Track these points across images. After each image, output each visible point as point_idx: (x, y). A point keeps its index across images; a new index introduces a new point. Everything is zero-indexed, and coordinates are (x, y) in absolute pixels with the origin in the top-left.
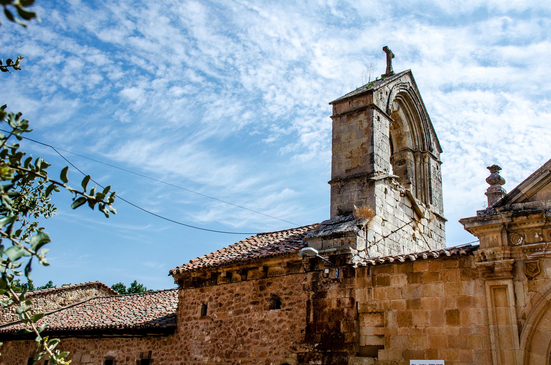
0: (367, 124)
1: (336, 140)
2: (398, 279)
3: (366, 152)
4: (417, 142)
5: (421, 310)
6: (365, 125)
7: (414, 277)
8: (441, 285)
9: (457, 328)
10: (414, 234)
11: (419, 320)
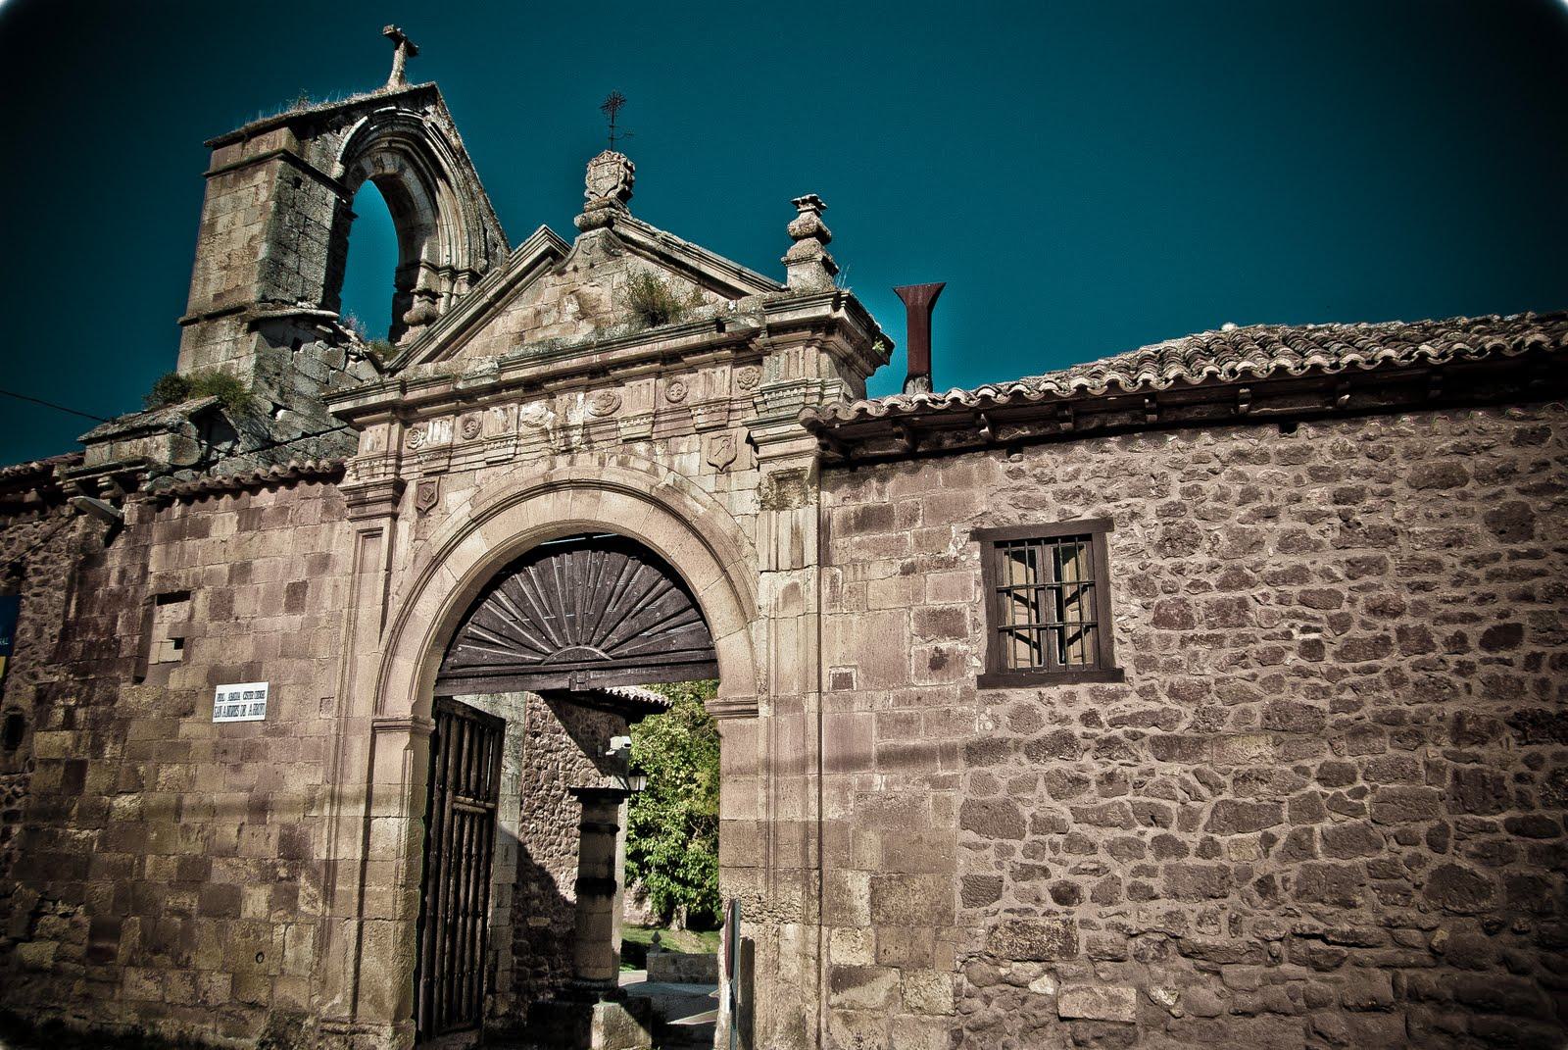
3: (255, 254)
9: (298, 618)
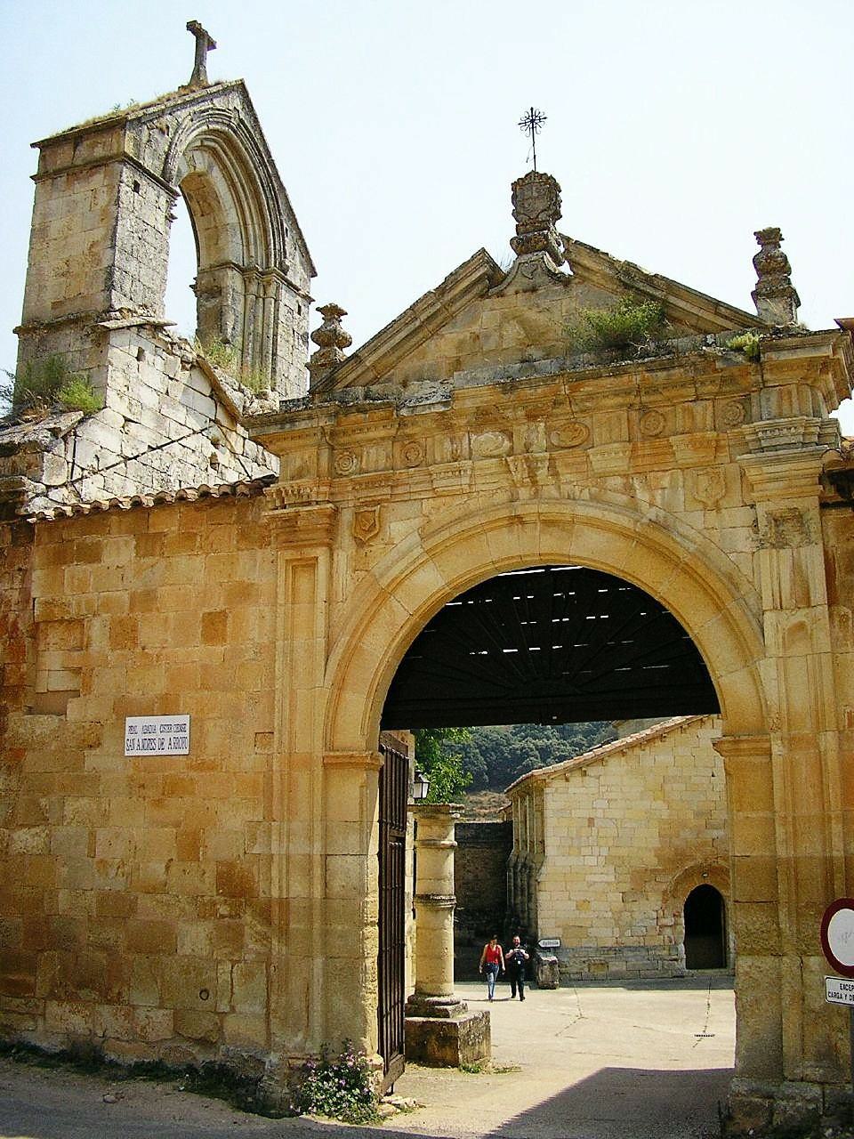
0: (107, 199)
1: (39, 233)
2: (118, 549)
4: (252, 247)
5: (157, 614)
6: (103, 199)
7: (149, 543)
8: (198, 559)
9: (219, 649)
10: (214, 455)
11: (150, 634)
